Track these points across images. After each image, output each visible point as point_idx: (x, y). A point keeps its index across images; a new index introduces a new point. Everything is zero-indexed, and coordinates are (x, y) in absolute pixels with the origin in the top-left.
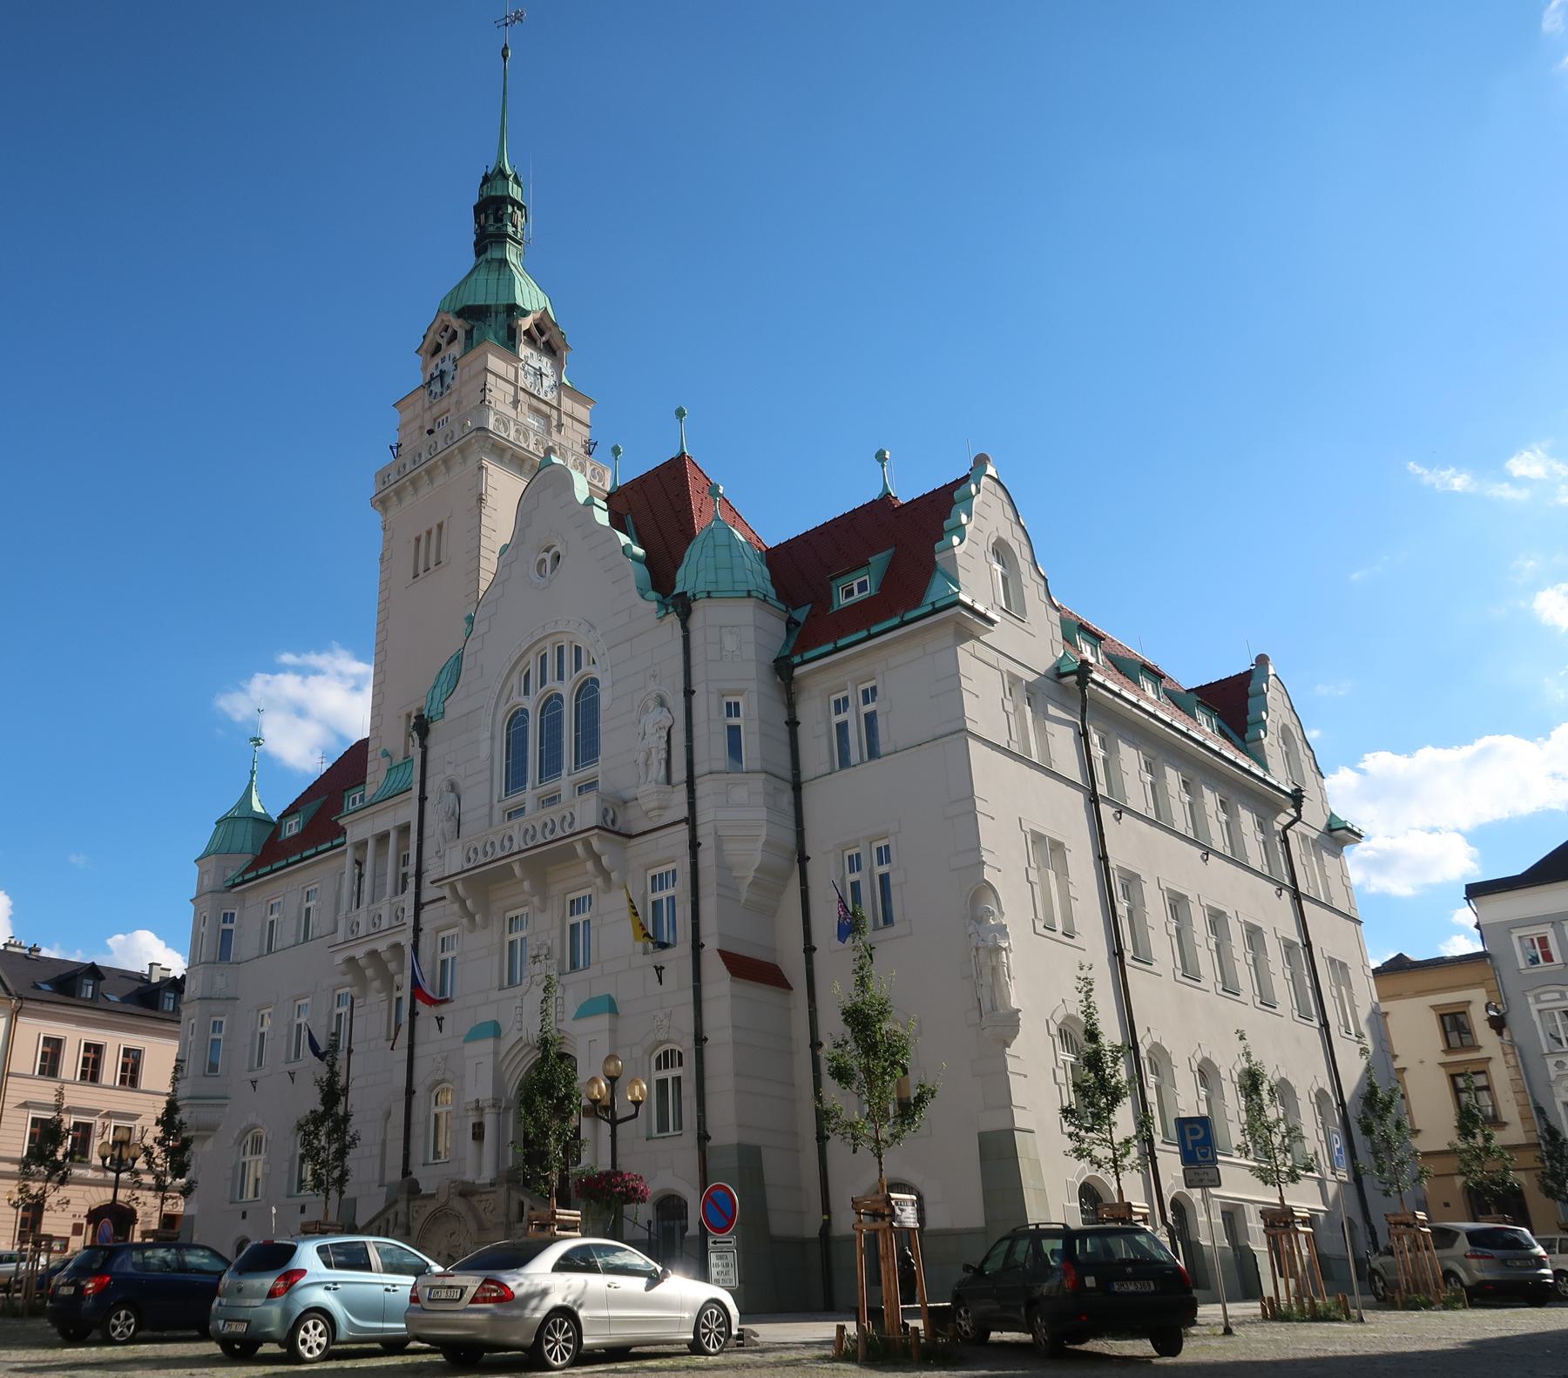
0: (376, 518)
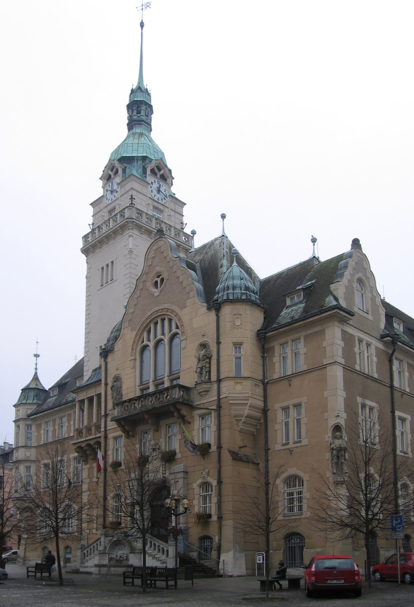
0: (83, 257)
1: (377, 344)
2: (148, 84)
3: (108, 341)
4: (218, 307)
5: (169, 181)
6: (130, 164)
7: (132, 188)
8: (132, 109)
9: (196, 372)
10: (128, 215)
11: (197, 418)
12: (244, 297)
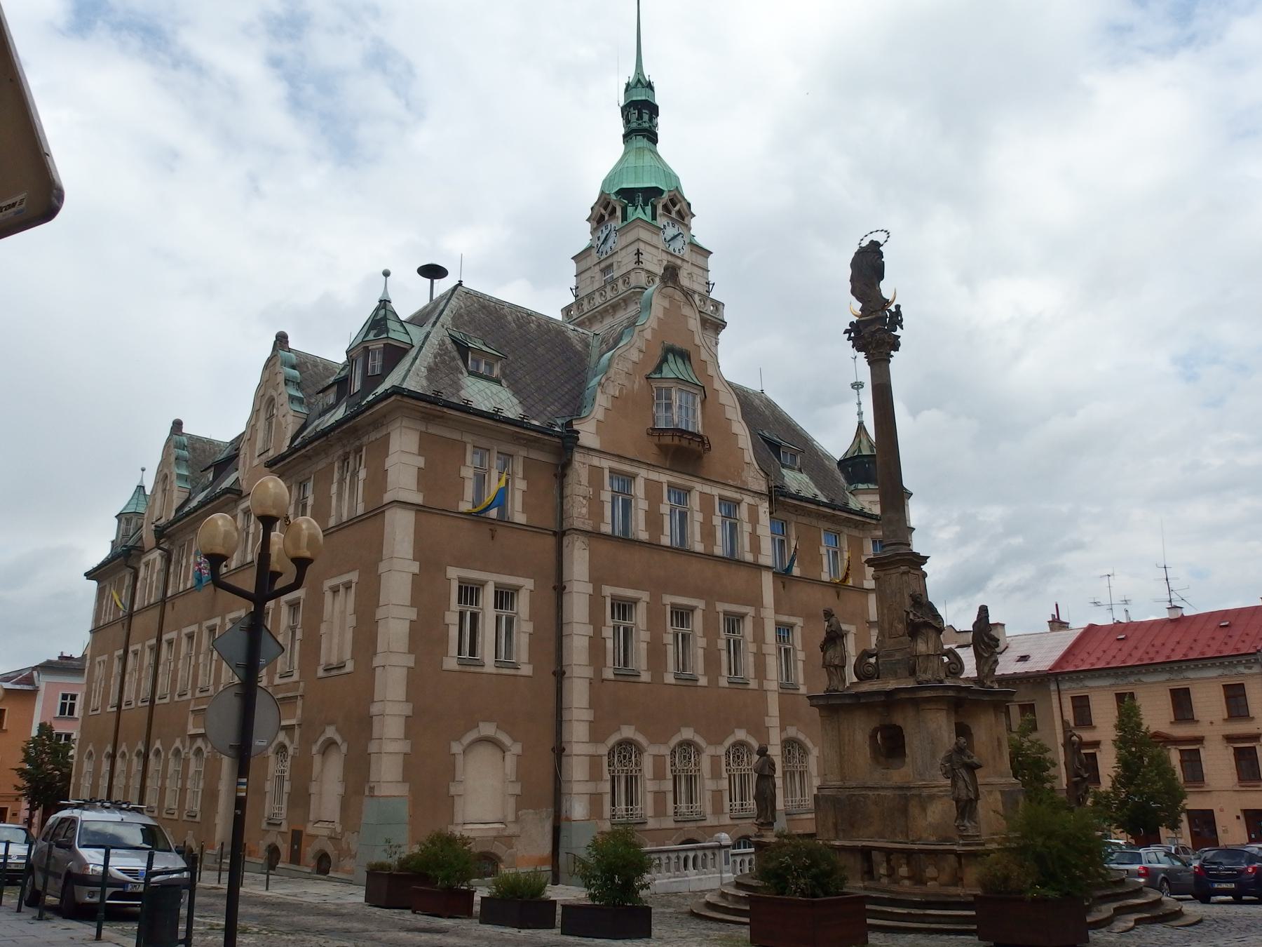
2: (649, 73)
7: (639, 239)
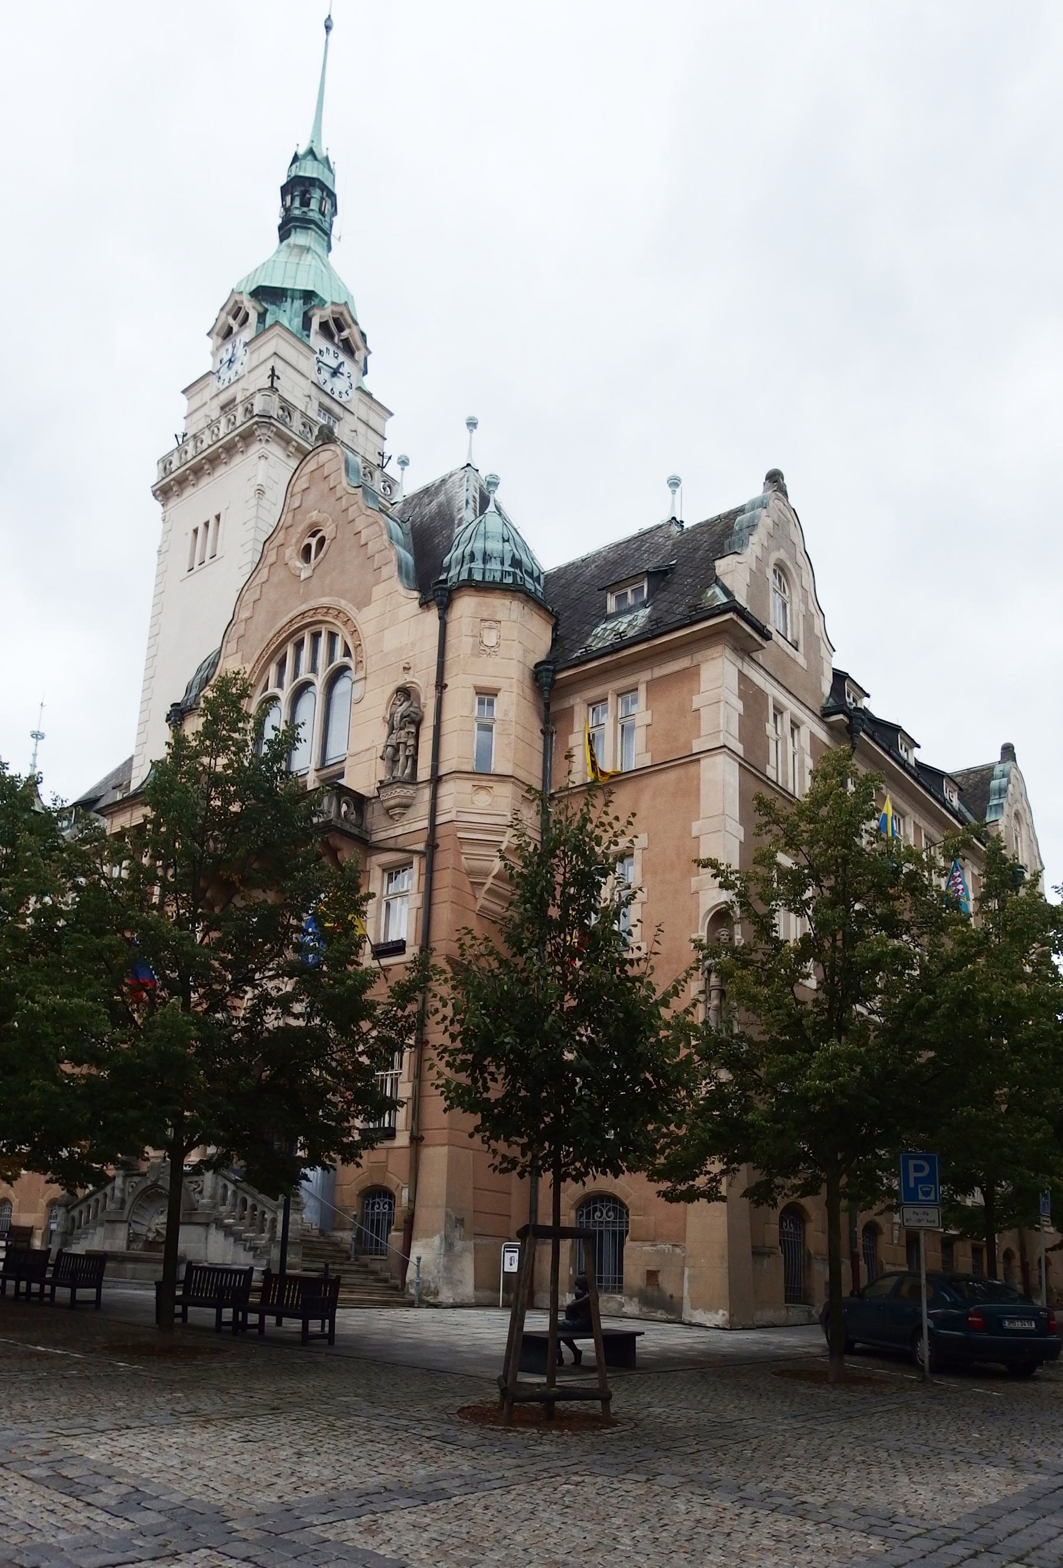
0: (157, 505)
1: (812, 726)
3: (188, 690)
4: (445, 599)
5: (359, 355)
6: (277, 306)
7: (275, 354)
8: (292, 194)
9: (382, 758)
10: (261, 409)
11: (376, 873)
12: (509, 580)
